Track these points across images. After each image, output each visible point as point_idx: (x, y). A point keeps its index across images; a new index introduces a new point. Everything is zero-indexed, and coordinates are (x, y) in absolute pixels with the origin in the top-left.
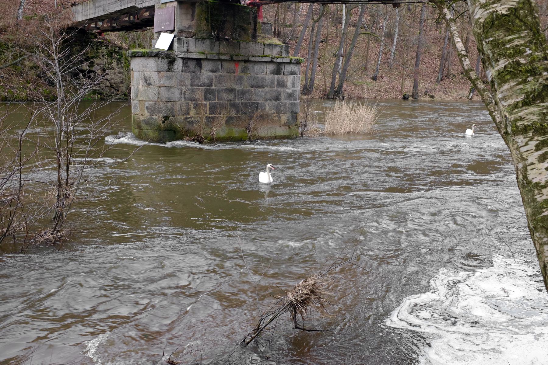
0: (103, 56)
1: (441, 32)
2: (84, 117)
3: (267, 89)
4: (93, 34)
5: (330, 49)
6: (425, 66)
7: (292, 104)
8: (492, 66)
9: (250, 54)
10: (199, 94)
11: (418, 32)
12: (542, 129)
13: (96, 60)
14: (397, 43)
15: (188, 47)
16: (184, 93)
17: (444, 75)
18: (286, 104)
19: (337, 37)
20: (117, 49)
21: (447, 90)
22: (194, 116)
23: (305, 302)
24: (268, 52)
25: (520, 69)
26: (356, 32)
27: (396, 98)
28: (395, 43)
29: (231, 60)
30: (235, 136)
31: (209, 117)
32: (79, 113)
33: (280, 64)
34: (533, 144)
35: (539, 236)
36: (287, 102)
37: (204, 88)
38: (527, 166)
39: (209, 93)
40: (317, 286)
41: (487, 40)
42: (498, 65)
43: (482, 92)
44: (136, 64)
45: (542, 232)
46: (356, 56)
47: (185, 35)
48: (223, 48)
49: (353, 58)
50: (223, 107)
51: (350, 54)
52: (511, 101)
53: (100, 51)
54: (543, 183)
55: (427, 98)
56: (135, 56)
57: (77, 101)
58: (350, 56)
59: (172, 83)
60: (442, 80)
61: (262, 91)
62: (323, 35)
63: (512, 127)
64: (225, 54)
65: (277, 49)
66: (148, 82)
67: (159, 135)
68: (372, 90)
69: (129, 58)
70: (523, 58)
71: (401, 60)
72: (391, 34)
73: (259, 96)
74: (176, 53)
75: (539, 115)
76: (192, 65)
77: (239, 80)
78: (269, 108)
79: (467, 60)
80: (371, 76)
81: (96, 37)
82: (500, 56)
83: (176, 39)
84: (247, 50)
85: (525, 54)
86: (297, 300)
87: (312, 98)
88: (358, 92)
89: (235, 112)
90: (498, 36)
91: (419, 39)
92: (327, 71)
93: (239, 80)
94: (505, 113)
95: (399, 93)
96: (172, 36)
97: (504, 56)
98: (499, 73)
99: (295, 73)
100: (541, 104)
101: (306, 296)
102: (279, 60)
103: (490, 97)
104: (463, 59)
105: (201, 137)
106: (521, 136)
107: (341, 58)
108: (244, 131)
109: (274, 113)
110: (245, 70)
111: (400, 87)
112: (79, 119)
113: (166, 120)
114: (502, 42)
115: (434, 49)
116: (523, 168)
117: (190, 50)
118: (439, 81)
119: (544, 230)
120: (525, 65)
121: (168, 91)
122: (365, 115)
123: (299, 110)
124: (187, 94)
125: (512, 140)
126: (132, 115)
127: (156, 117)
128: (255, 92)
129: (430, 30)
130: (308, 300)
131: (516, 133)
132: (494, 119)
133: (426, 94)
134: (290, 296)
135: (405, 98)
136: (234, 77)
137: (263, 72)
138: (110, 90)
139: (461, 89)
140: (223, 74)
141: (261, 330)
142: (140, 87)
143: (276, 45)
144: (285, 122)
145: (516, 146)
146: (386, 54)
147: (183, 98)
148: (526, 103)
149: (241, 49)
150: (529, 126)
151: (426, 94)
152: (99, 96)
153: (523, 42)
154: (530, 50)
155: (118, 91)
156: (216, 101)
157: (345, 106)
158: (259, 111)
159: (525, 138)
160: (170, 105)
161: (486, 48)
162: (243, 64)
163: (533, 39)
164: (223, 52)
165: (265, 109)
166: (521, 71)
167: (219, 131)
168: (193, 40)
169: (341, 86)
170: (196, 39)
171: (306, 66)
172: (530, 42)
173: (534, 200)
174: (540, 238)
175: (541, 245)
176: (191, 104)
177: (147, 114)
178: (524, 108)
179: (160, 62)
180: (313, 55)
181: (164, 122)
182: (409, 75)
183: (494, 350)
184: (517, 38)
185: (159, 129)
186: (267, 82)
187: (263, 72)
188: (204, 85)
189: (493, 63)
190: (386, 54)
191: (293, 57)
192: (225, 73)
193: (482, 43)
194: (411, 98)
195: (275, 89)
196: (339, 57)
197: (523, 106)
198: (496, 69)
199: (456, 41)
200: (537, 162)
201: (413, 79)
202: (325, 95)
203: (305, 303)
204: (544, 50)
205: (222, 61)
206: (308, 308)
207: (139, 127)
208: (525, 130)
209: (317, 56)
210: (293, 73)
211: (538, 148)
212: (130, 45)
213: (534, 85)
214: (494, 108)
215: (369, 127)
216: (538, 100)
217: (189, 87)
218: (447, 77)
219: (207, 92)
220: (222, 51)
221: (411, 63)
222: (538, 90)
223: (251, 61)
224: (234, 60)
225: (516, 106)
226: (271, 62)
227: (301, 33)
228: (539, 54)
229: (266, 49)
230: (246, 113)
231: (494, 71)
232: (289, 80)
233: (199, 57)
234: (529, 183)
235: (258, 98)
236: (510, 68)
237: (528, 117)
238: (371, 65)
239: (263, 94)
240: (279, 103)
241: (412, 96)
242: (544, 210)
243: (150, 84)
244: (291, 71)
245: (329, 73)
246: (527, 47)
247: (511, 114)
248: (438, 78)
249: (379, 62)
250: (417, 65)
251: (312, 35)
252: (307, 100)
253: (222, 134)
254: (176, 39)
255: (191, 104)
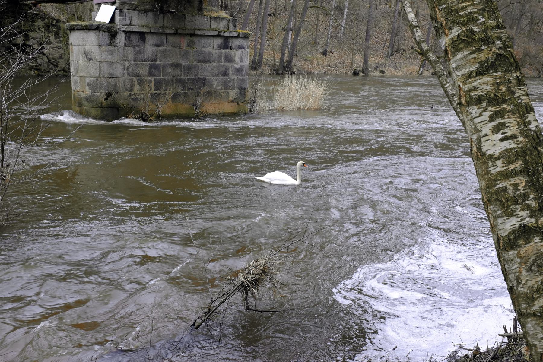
0: (39, 29)
1: (390, 6)
2: (20, 93)
3: (214, 64)
4: (27, 5)
5: (280, 23)
6: (375, 40)
7: (240, 79)
8: (445, 34)
9: (196, 27)
10: (144, 70)
11: (368, 5)
12: (495, 99)
13: (32, 34)
14: (347, 18)
15: (131, 20)
16: (128, 69)
17: (395, 50)
18: (234, 80)
19: (286, 10)
20: (55, 21)
21: (398, 65)
22: (138, 92)
23: (256, 282)
24: (214, 25)
25: (474, 37)
26: (305, 6)
27: (347, 73)
28: (345, 17)
29: (177, 33)
30: (181, 113)
31: (154, 94)
32: (14, 88)
33: (227, 38)
34: (487, 114)
35: (493, 209)
36: (236, 77)
37: (148, 63)
38: (481, 137)
39: (153, 69)
40: (268, 266)
41: (440, 7)
42: (451, 33)
43: (434, 64)
44: (75, 38)
45: (496, 205)
46: (305, 30)
47: (127, 7)
48: (168, 21)
49: (302, 32)
50: (167, 83)
51: (299, 28)
52: (465, 71)
53: (36, 24)
54: (497, 154)
55: (377, 73)
56: (74, 30)
57: (11, 77)
58: (300, 30)
59: (115, 58)
60: (392, 55)
61: (209, 66)
62: (271, 8)
63: (466, 97)
64: (169, 28)
65: (224, 23)
66: (88, 58)
67: (102, 112)
68: (322, 65)
69: (68, 32)
70: (476, 26)
71: (351, 34)
72: (341, 8)
73: (206, 71)
74: (118, 27)
75: (493, 85)
76: (135, 39)
77: (185, 55)
78: (216, 83)
79: (419, 31)
80: (321, 51)
81: (30, 8)
82: (454, 24)
83: (117, 11)
84: (193, 23)
85: (478, 22)
86: (248, 280)
87: (261, 74)
88: (307, 67)
89: (182, 88)
90: (451, 3)
91: (370, 13)
92: (276, 46)
93: (185, 55)
94: (459, 83)
95: (349, 69)
96: (113, 8)
97: (458, 24)
98: (453, 41)
99: (243, 48)
100: (495, 74)
101: (258, 277)
102: (226, 34)
103: (442, 69)
104: (415, 30)
105: (146, 115)
106: (475, 107)
107: (291, 32)
108: (191, 107)
109: (222, 89)
110: (191, 45)
111: (350, 62)
112: (13, 96)
113: (108, 97)
114: (456, 9)
115: (384, 23)
116: (477, 139)
117: (133, 23)
118: (389, 56)
119: (498, 203)
120: (478, 33)
121: (111, 67)
122: (314, 92)
123: (247, 85)
124: (130, 69)
125: (466, 111)
126: (73, 92)
127: (98, 94)
128: (202, 68)
129: (380, 5)
130: (259, 280)
131: (470, 103)
132: (446, 92)
133: (376, 69)
134: (241, 277)
135: (356, 73)
136: (180, 51)
137: (210, 46)
138: (48, 66)
139: (411, 64)
140: (168, 48)
141: (212, 313)
142: (81, 62)
143: (223, 18)
144: (234, 98)
145: (470, 117)
146: (336, 28)
147: (126, 74)
148: (480, 73)
149: (186, 23)
150: (483, 96)
151: (376, 69)
152: (36, 72)
153: (476, 10)
154: (483, 18)
155: (57, 66)
156: (162, 77)
157: (294, 81)
158: (206, 87)
159: (479, 109)
160: (112, 81)
161: (440, 16)
162: (189, 38)
163: (486, 7)
164: (168, 25)
165: (212, 85)
166: (474, 39)
167: (164, 107)
168: (136, 12)
169: (290, 61)
170: (139, 11)
171: (255, 41)
172: (483, 10)
173: (488, 173)
174: (494, 211)
175: (495, 218)
176: (135, 79)
177: (88, 91)
178: (478, 78)
179: (101, 36)
180: (261, 29)
181: (106, 99)
182: (359, 50)
183: (448, 325)
184: (471, 5)
185: (101, 107)
186: (214, 57)
187: (210, 46)
188: (148, 60)
189: (447, 32)
190: (336, 28)
191: (240, 31)
192: (170, 48)
193: (435, 11)
194: (361, 74)
195: (223, 64)
196: (288, 31)
197: (476, 76)
198: (450, 37)
199: (407, 11)
200: (490, 133)
201: (363, 53)
202: (274, 70)
203: (256, 284)
204: (497, 18)
205: (167, 34)
206: (260, 288)
207: (80, 105)
208: (479, 100)
209: (266, 30)
210: (241, 47)
211: (492, 118)
212: (69, 18)
213: (488, 54)
214: (446, 80)
215: (320, 103)
216: (492, 69)
217: (133, 62)
218: (397, 51)
219: (152, 67)
220: (166, 24)
221: (361, 38)
222: (492, 59)
223: (198, 35)
224: (180, 34)
225: (470, 75)
226: (218, 36)
227: (249, 7)
228: (492, 22)
229: (212, 22)
230: (192, 89)
231: (447, 39)
232: (237, 54)
233: (142, 31)
234: (483, 155)
235: (205, 73)
236: (464, 37)
237: (482, 87)
238: (321, 40)
239: (210, 69)
240: (227, 79)
241: (363, 72)
242: (498, 182)
243: (91, 59)
244: (239, 46)
245: (278, 47)
246: (480, 14)
247: (465, 84)
248: (388, 53)
249: (329, 37)
250: (367, 40)
251: (260, 8)
252: (256, 75)
253: (168, 112)
254: (117, 11)
255: (135, 79)
